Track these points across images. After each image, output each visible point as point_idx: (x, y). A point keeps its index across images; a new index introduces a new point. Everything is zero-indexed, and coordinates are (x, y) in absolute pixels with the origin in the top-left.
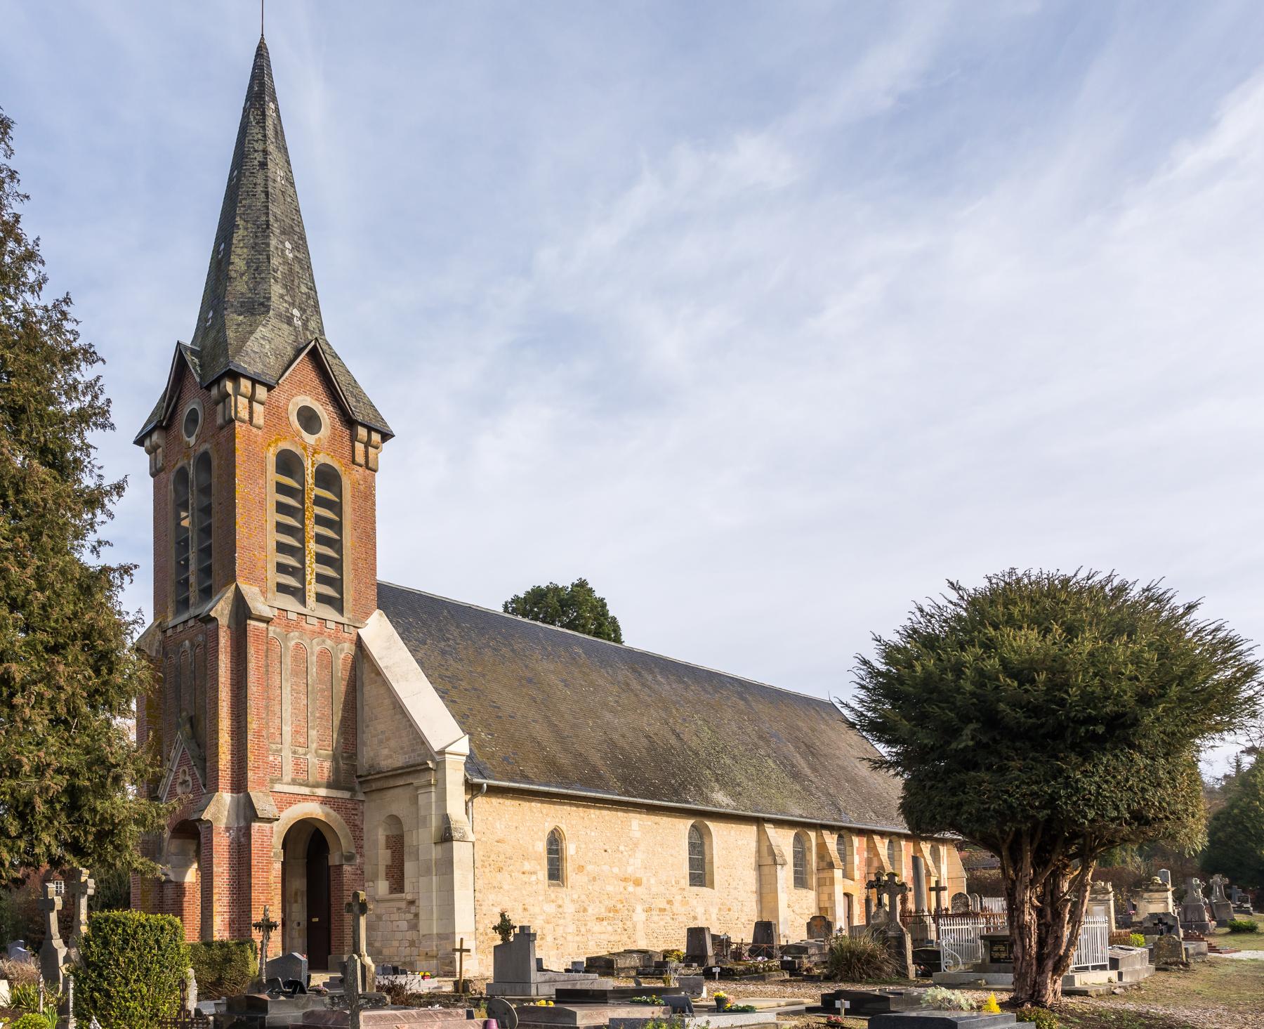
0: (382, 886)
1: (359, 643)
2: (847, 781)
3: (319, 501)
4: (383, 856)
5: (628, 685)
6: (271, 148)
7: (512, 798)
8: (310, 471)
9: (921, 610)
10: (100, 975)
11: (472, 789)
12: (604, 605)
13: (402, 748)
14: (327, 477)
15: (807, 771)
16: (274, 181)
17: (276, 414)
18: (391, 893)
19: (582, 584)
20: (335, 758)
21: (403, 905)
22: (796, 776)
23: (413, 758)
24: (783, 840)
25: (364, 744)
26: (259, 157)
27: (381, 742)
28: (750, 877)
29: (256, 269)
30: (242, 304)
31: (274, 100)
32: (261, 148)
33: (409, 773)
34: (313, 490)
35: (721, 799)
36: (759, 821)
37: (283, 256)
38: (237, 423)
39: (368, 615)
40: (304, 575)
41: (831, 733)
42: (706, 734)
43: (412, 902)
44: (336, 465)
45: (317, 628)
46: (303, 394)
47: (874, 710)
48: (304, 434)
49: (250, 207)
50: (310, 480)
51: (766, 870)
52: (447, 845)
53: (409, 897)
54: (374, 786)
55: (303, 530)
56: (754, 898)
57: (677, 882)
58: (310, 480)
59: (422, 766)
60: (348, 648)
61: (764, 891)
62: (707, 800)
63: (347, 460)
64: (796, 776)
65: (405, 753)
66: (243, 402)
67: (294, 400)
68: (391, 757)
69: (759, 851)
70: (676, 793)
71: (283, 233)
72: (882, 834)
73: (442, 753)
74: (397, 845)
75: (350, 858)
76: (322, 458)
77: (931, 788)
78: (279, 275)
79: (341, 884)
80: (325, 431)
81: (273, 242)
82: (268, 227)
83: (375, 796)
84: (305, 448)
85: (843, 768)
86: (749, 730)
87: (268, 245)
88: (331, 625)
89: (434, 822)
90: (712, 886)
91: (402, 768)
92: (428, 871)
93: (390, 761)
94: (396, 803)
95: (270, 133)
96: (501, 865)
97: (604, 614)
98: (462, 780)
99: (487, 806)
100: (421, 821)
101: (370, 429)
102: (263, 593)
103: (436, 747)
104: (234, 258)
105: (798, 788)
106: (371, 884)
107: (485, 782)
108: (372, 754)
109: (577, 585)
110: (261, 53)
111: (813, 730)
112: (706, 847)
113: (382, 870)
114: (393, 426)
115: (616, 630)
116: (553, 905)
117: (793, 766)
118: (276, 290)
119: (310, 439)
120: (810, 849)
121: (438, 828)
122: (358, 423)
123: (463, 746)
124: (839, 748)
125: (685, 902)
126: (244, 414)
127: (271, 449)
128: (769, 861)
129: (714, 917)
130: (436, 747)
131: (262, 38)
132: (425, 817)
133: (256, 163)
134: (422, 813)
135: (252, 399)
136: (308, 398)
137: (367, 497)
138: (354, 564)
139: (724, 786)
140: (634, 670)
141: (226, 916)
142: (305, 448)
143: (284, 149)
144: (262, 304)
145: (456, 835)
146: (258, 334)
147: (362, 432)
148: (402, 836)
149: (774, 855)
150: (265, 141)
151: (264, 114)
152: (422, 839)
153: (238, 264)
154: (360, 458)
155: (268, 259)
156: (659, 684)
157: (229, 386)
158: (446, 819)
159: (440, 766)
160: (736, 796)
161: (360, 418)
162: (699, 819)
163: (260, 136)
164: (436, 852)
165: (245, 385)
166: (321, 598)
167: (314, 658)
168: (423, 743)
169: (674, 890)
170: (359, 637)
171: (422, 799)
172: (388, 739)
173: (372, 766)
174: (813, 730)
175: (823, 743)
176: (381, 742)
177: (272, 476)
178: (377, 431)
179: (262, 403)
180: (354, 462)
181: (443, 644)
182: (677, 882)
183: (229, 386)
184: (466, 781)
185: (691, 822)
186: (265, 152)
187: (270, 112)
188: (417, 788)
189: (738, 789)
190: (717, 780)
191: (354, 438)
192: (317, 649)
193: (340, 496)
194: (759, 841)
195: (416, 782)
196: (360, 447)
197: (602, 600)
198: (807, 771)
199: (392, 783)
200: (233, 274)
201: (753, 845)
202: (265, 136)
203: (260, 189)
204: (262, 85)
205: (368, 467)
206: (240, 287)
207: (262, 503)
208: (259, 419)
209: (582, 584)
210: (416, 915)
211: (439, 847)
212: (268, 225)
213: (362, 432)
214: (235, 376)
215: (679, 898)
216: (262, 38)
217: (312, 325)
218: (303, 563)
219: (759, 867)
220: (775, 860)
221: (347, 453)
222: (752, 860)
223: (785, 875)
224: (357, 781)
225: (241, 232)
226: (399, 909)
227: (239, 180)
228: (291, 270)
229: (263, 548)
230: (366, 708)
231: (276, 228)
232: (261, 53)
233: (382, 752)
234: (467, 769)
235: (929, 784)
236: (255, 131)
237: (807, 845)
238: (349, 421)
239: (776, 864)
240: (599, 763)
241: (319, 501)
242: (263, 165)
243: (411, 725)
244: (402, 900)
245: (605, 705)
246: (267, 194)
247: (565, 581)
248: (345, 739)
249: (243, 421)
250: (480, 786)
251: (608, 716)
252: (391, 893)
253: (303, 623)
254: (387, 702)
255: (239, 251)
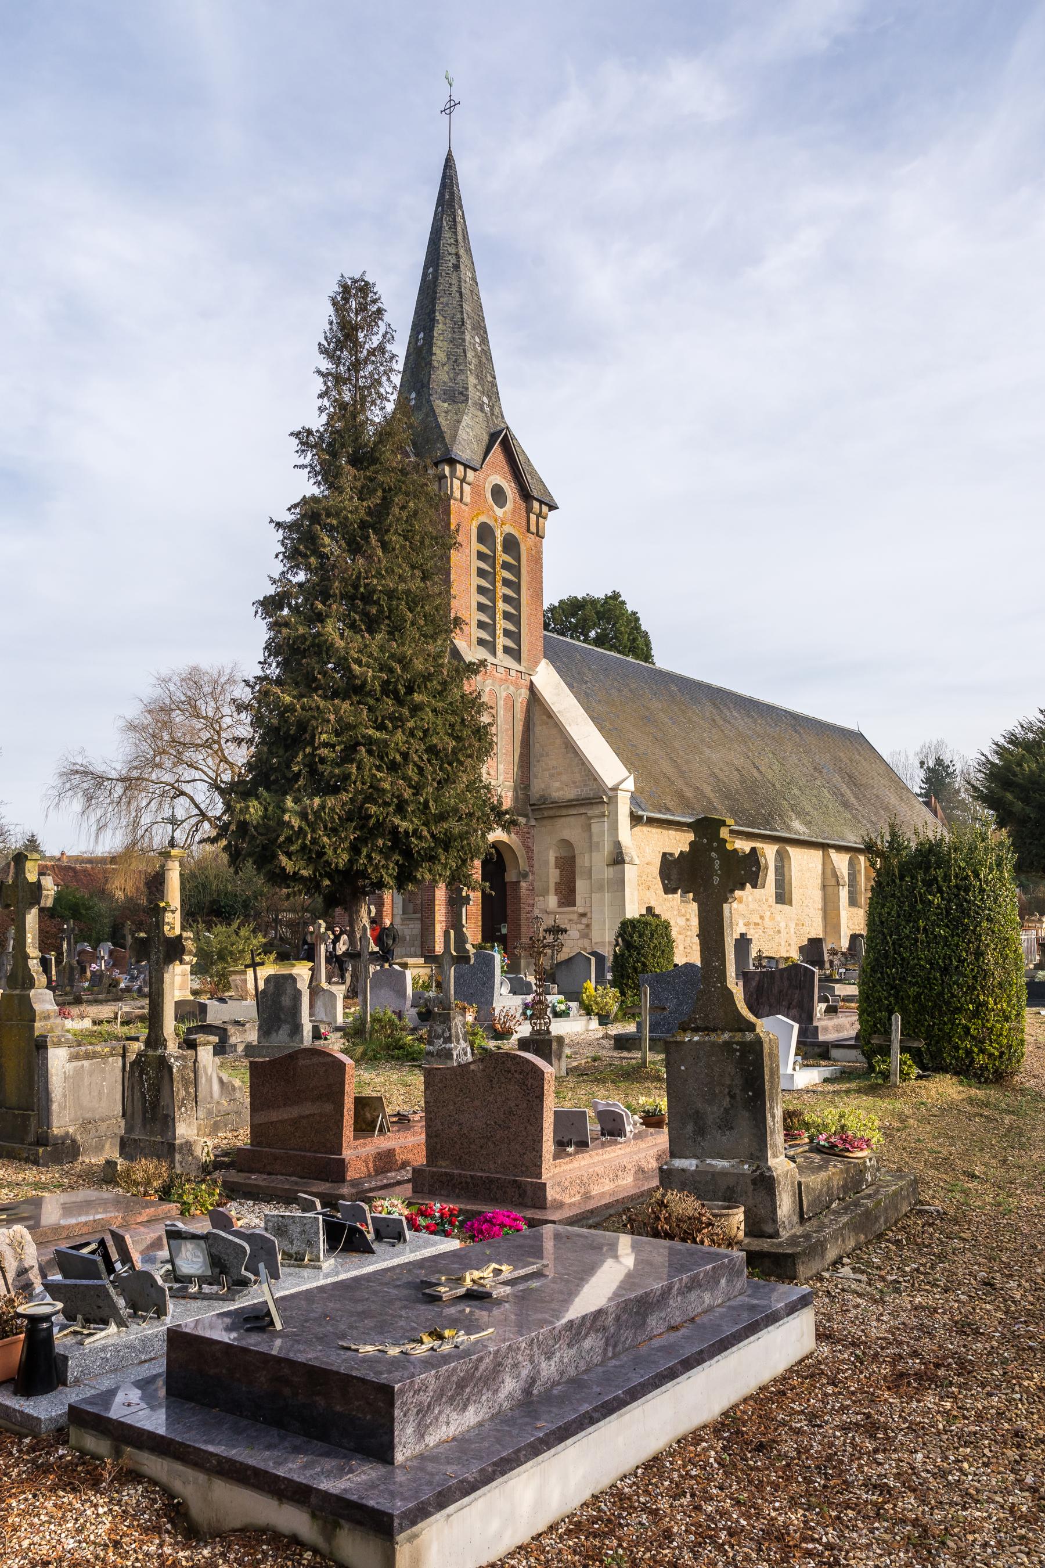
0: (552, 901)
1: (532, 687)
2: (883, 809)
3: (506, 566)
4: (554, 875)
5: (714, 720)
6: (462, 252)
7: (657, 827)
8: (499, 540)
9: (1022, 726)
10: (638, 954)
11: (636, 820)
12: (637, 620)
13: (574, 782)
14: (511, 544)
15: (853, 800)
16: (465, 281)
17: (477, 491)
18: (559, 906)
19: (616, 596)
20: (515, 790)
21: (575, 917)
22: (846, 805)
23: (586, 792)
24: (841, 861)
25: (536, 777)
26: (453, 260)
27: (552, 776)
28: (818, 895)
29: (455, 361)
30: (445, 392)
31: (461, 208)
32: (454, 252)
33: (582, 805)
34: (502, 557)
35: (799, 828)
36: (824, 847)
37: (475, 350)
38: (452, 502)
39: (537, 663)
40: (495, 630)
41: (865, 763)
42: (776, 767)
43: (584, 915)
44: (516, 534)
45: (503, 676)
46: (498, 476)
47: (986, 788)
48: (496, 508)
49: (447, 304)
50: (499, 548)
51: (830, 890)
52: (619, 867)
53: (581, 910)
54: (546, 814)
55: (494, 591)
56: (820, 914)
57: (767, 900)
58: (499, 548)
59: (595, 799)
60: (524, 693)
61: (828, 908)
62: (789, 828)
63: (524, 529)
64: (846, 805)
65: (577, 787)
66: (456, 483)
67: (492, 477)
68: (563, 789)
69: (824, 873)
70: (767, 822)
71: (473, 329)
72: (839, 848)
73: (615, 789)
74: (568, 867)
75: (525, 876)
76: (508, 529)
77: (1030, 844)
78: (472, 367)
79: (518, 898)
80: (509, 505)
81: (468, 338)
82: (463, 324)
83: (545, 822)
84: (496, 521)
85: (878, 797)
86: (806, 762)
87: (464, 340)
88: (513, 673)
89: (607, 847)
90: (790, 904)
91: (577, 800)
92: (601, 888)
93: (561, 792)
94: (569, 829)
95: (460, 238)
96: (649, 883)
97: (637, 628)
98: (628, 812)
99: (640, 833)
100: (592, 846)
101: (541, 503)
102: (470, 646)
103: (610, 784)
104: (435, 350)
105: (849, 816)
106: (541, 898)
107: (646, 814)
108: (543, 786)
109: (610, 597)
110: (449, 163)
111: (851, 760)
112: (786, 869)
113: (552, 886)
114: (558, 499)
115: (648, 644)
116: (684, 919)
117: (843, 796)
118: (472, 380)
119: (499, 512)
120: (860, 871)
121: (610, 853)
122: (533, 497)
123: (630, 785)
124: (872, 778)
125: (772, 918)
126: (457, 494)
127: (474, 522)
128: (833, 882)
129: (792, 931)
130: (610, 784)
131: (450, 151)
132: (598, 843)
133: (450, 265)
134: (595, 839)
135: (463, 481)
136: (498, 477)
137: (537, 560)
138: (528, 619)
139: (798, 815)
140: (716, 707)
141: (444, 924)
142: (496, 521)
143: (469, 251)
144: (461, 393)
145: (627, 858)
146: (464, 423)
147: (536, 505)
148: (574, 857)
149: (837, 877)
150: (457, 246)
151: (454, 220)
152: (597, 861)
153: (439, 354)
154: (533, 529)
155: (465, 352)
156: (736, 719)
157: (447, 470)
158: (618, 845)
159: (613, 800)
160: (808, 824)
161: (535, 494)
162: (782, 845)
163: (452, 241)
164: (608, 873)
165: (460, 468)
166: (507, 650)
167: (502, 702)
168: (595, 779)
169: (765, 907)
170: (531, 682)
171: (595, 828)
172: (560, 774)
173: (542, 796)
174: (851, 760)
175: (860, 773)
176: (552, 776)
177: (475, 546)
178: (546, 504)
179: (469, 484)
180: (528, 530)
181: (584, 686)
182: (767, 900)
183: (447, 469)
184: (631, 813)
185: (776, 847)
186: (457, 255)
187: (459, 219)
188: (590, 818)
189: (809, 818)
190: (793, 810)
191: (529, 510)
192: (504, 694)
193: (519, 560)
194: (824, 864)
195: (590, 813)
196: (533, 517)
197: (634, 614)
198: (853, 800)
199: (564, 812)
200: (435, 364)
201: (820, 867)
202: (456, 241)
203: (454, 289)
204: (452, 194)
205: (538, 535)
206: (441, 376)
207: (468, 569)
208: (467, 498)
209: (616, 596)
210: (588, 926)
211: (611, 869)
212: (463, 322)
213: (536, 505)
214: (452, 462)
215: (768, 913)
216: (450, 151)
217: (496, 410)
218: (494, 620)
219: (824, 887)
220: (838, 881)
221: (524, 523)
222: (818, 881)
223: (844, 893)
224: (529, 808)
225: (440, 326)
226: (570, 920)
227: (435, 279)
228: (480, 362)
229: (468, 608)
230: (537, 745)
231: (468, 326)
232: (449, 163)
233: (559, 787)
234: (631, 803)
235: (1028, 841)
236: (447, 234)
237: (857, 867)
238: (526, 495)
239: (838, 884)
240: (711, 795)
241: (506, 566)
242: (457, 267)
243: (583, 764)
244: (573, 912)
245: (703, 740)
246: (461, 294)
247: (599, 593)
248: (522, 772)
249: (456, 500)
250: (641, 817)
251: (707, 751)
252: (559, 906)
253: (494, 672)
254: (558, 742)
255: (439, 343)
